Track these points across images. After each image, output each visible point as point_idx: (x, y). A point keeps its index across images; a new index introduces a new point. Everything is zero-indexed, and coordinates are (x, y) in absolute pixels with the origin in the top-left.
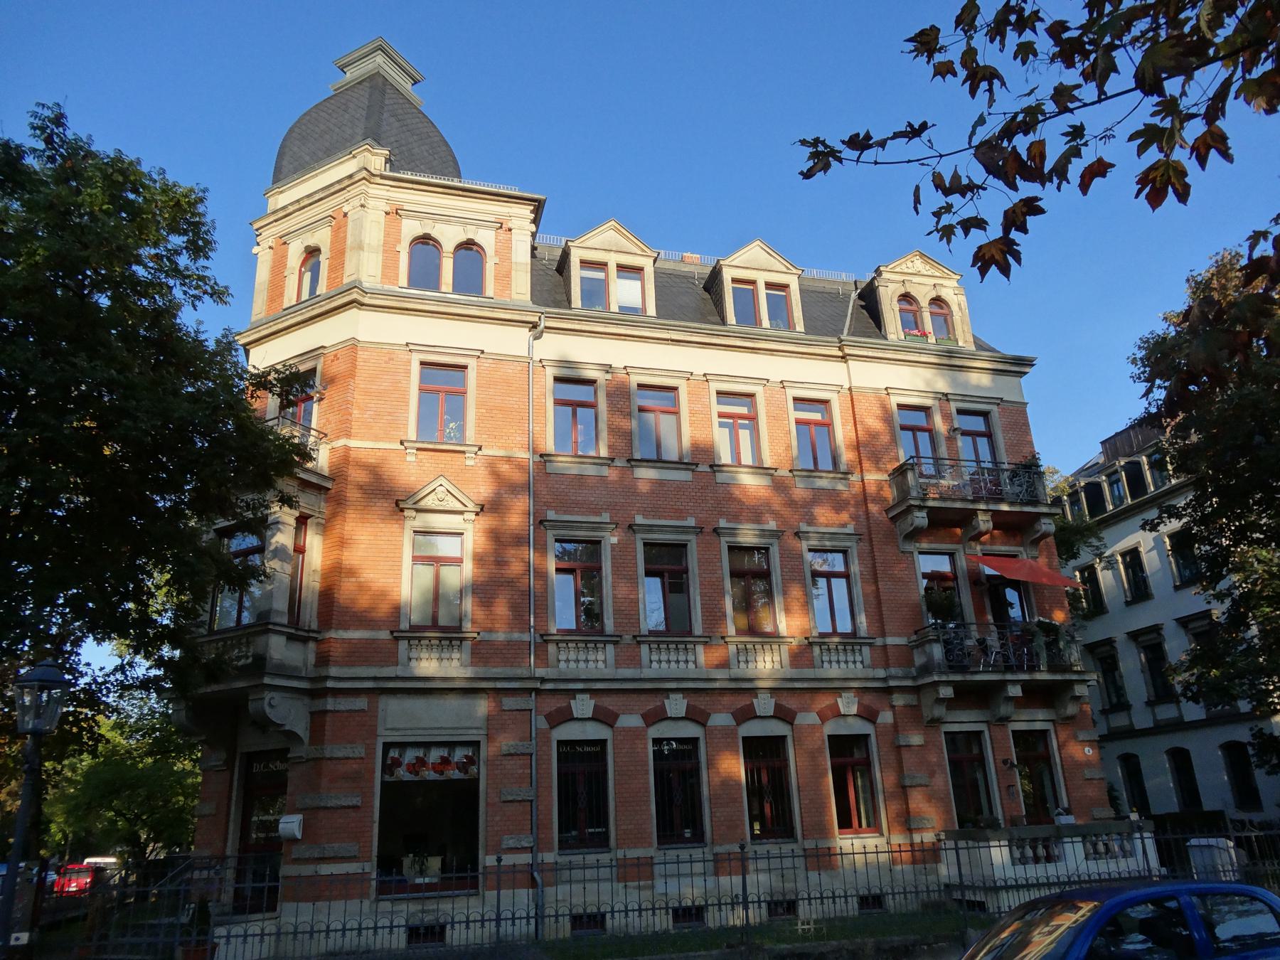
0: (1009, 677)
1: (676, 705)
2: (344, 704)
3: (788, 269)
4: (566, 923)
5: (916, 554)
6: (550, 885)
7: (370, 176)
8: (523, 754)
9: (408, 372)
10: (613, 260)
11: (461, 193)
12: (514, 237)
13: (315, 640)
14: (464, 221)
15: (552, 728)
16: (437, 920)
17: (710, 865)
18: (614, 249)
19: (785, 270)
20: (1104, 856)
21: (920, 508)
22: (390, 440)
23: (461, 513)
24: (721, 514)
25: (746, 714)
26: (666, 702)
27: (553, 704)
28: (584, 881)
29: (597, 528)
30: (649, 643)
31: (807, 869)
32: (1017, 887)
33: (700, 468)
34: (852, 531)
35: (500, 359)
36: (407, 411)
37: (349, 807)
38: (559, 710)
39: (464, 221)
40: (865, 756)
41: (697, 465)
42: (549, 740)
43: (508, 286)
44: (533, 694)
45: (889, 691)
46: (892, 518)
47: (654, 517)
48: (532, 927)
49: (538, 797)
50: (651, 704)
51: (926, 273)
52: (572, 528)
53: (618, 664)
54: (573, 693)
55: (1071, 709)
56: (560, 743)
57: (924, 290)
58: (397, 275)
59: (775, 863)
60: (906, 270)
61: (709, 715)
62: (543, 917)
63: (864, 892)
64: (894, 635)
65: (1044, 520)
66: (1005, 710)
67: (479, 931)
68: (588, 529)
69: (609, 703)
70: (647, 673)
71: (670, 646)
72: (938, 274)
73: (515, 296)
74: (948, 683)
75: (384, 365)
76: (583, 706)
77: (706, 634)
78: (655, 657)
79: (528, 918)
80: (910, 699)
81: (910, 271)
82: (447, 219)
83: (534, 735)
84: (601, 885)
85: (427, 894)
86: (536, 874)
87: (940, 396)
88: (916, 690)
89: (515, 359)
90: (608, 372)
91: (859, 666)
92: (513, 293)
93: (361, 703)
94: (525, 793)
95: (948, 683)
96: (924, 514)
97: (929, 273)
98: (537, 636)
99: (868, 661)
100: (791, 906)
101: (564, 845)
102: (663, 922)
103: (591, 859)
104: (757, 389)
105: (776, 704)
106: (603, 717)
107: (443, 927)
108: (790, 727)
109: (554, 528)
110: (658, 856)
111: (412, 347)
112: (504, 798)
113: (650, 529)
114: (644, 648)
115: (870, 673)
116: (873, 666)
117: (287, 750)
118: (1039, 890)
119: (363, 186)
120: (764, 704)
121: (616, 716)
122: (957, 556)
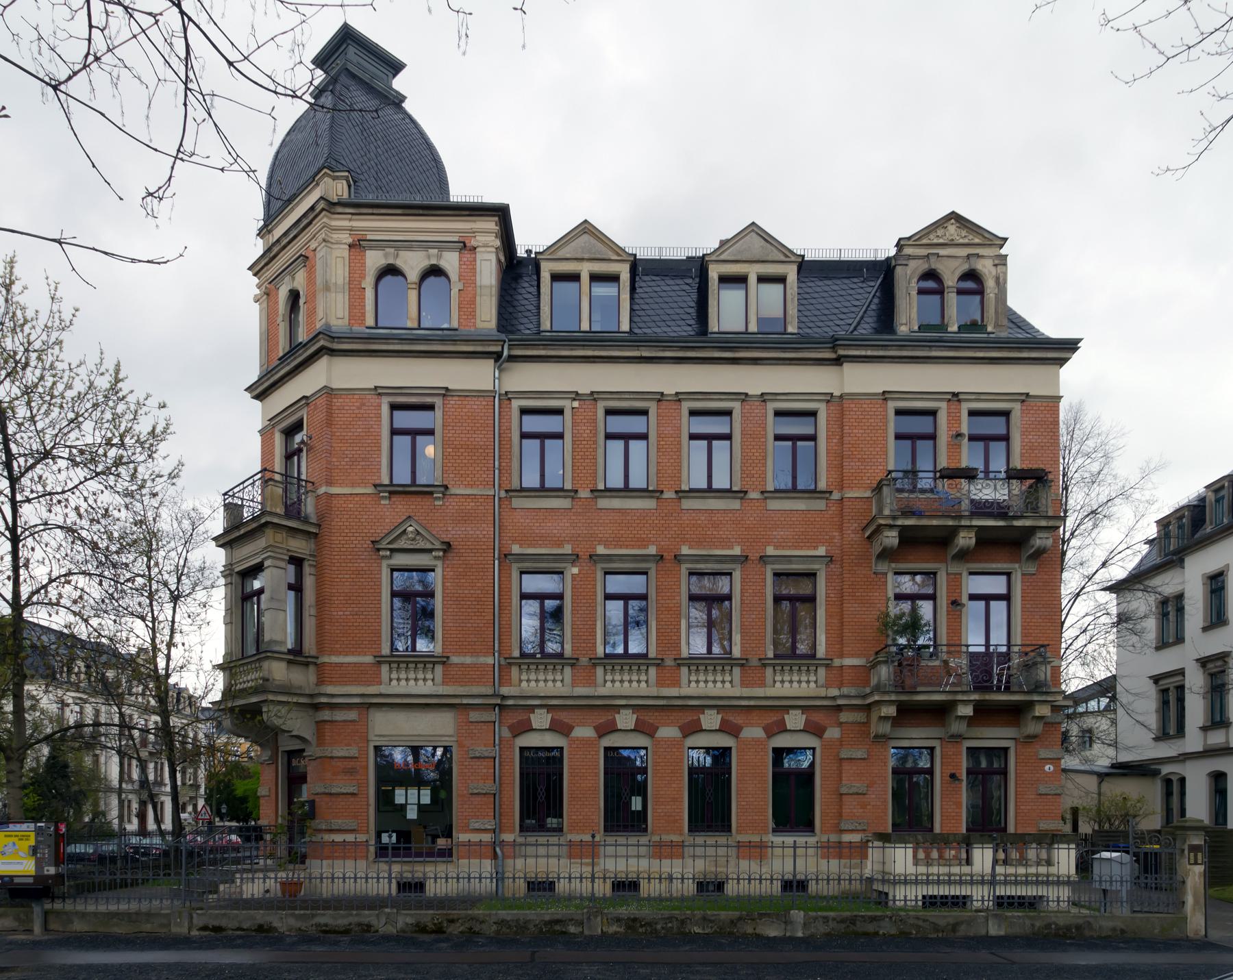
0: (1036, 698)
1: (711, 720)
2: (340, 716)
3: (787, 256)
4: (522, 885)
5: (965, 574)
6: (509, 857)
7: (331, 206)
8: (487, 758)
9: (379, 416)
10: (585, 269)
11: (421, 212)
12: (479, 256)
13: (315, 664)
14: (424, 245)
15: (514, 737)
16: (413, 878)
17: (565, 849)
18: (586, 256)
19: (783, 258)
20: (935, 863)
21: (891, 527)
22: (362, 483)
23: (430, 551)
24: (684, 541)
25: (608, 729)
26: (702, 716)
27: (602, 718)
28: (537, 856)
29: (535, 559)
30: (390, 663)
31: (738, 857)
32: (916, 882)
33: (666, 495)
34: (824, 554)
35: (466, 395)
36: (379, 456)
37: (347, 794)
38: (520, 722)
39: (424, 245)
40: (1003, 766)
41: (662, 492)
42: (512, 747)
43: (473, 314)
44: (497, 709)
45: (839, 708)
46: (869, 538)
47: (615, 547)
48: (494, 885)
49: (500, 791)
50: (602, 718)
51: (961, 241)
52: (790, 562)
53: (574, 684)
54: (532, 708)
55: (1033, 728)
56: (606, 749)
57: (953, 264)
58: (363, 315)
59: (710, 851)
60: (935, 241)
61: (657, 728)
62: (503, 879)
63: (788, 877)
64: (852, 656)
65: (1040, 535)
66: (957, 727)
67: (455, 885)
68: (548, 561)
69: (564, 717)
70: (602, 691)
71: (726, 668)
72: (977, 241)
73: (480, 325)
74: (891, 702)
75: (357, 411)
76: (541, 719)
77: (660, 657)
78: (609, 677)
79: (491, 878)
80: (859, 717)
81: (941, 241)
82: (408, 245)
83: (497, 742)
84: (550, 860)
85: (427, 859)
86: (498, 849)
87: (949, 397)
88: (868, 708)
89: (480, 394)
90: (574, 399)
91: (812, 685)
92: (478, 321)
93: (352, 715)
94: (489, 787)
95: (891, 702)
96: (894, 533)
97: (966, 241)
98: (502, 659)
99: (822, 680)
100: (720, 886)
101: (523, 829)
102: (603, 889)
103: (633, 840)
104: (566, 404)
105: (722, 719)
106: (557, 727)
107: (552, 883)
108: (735, 740)
109: (517, 561)
110: (689, 840)
111: (380, 391)
112: (471, 791)
113: (608, 558)
114: (769, 671)
115: (822, 692)
116: (827, 686)
117: (303, 750)
118: (883, 884)
119: (324, 219)
120: (626, 720)
121: (571, 728)
122: (1013, 577)
